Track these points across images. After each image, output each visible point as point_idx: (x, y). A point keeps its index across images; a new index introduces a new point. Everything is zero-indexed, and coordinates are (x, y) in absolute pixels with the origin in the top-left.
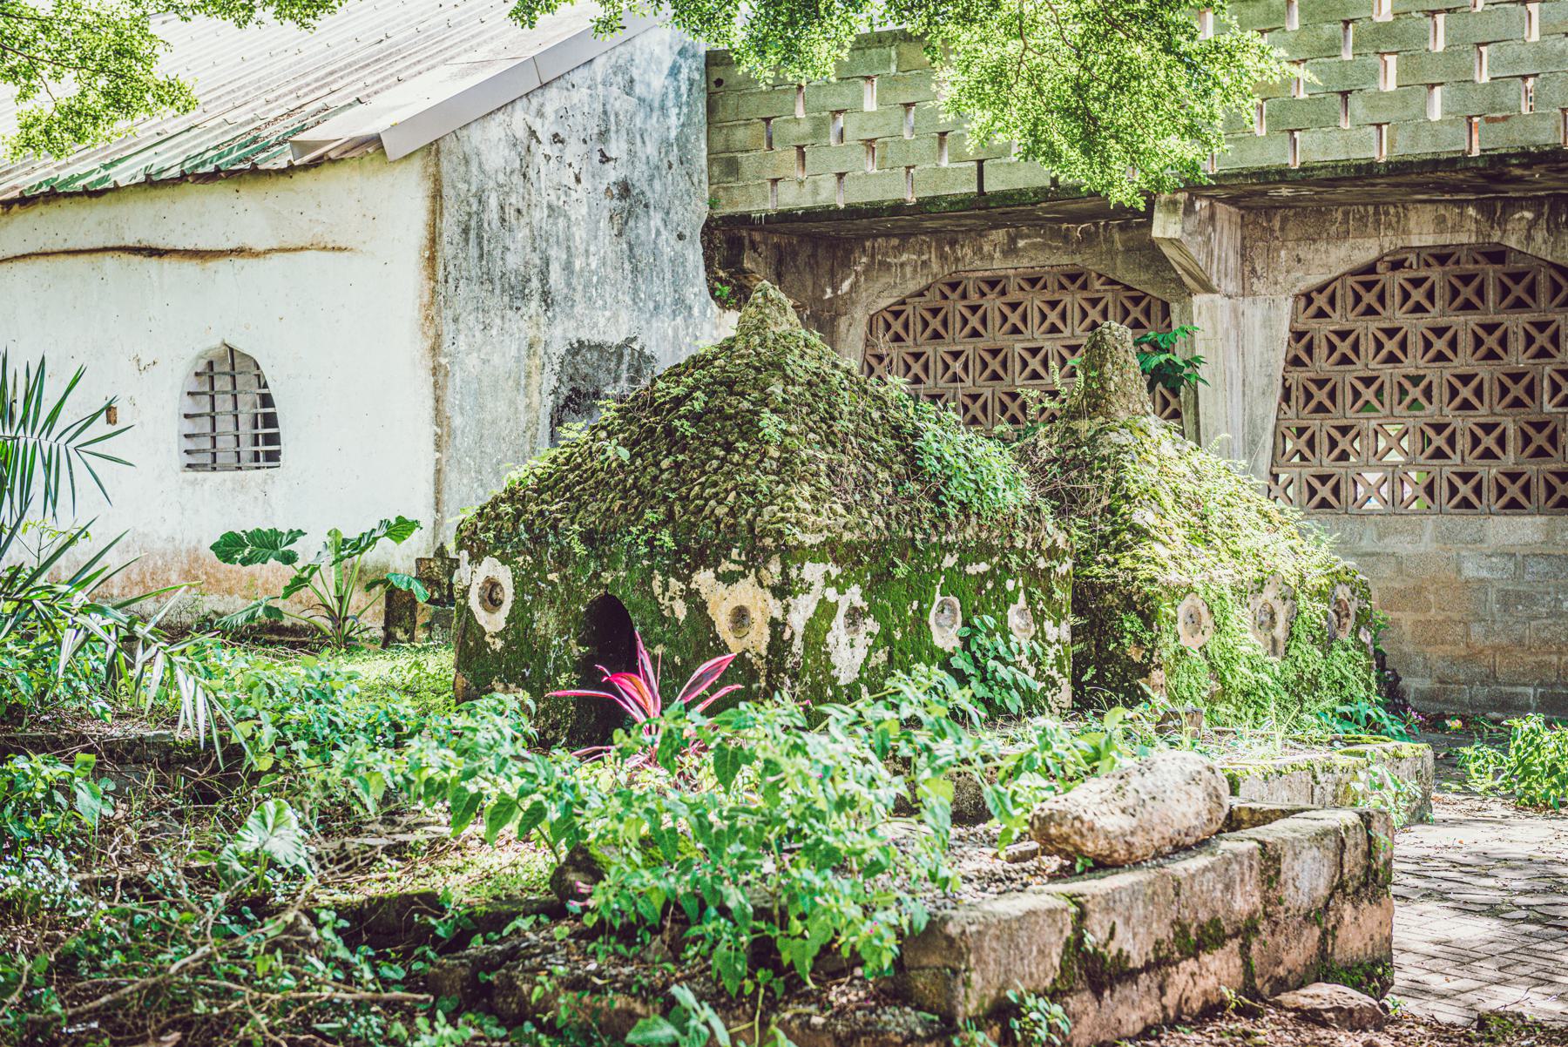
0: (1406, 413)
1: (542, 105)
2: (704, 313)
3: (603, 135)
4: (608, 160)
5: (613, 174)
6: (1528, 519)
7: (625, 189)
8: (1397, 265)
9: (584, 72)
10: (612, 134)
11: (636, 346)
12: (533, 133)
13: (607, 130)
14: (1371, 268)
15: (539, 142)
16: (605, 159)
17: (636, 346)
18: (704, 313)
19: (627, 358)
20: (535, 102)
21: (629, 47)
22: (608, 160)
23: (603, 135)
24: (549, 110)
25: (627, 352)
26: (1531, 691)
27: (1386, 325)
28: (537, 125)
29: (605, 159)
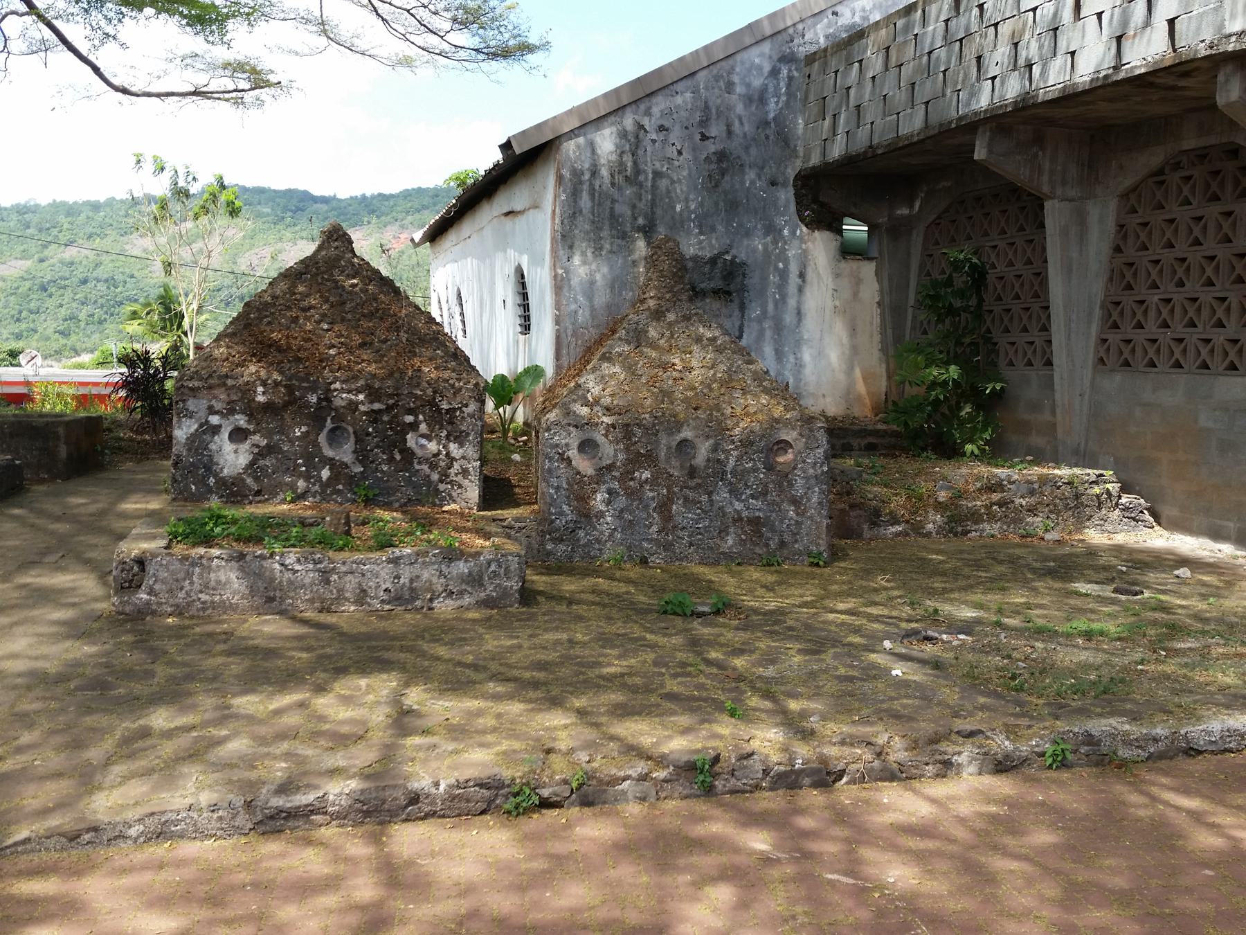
0: (1176, 289)
1: (650, 108)
2: (793, 233)
3: (704, 122)
4: (708, 138)
5: (711, 147)
6: (1239, 379)
7: (722, 156)
8: (1177, 166)
9: (688, 82)
10: (713, 121)
11: (728, 257)
12: (642, 127)
13: (708, 119)
14: (1160, 172)
15: (646, 131)
16: (704, 138)
17: (728, 257)
18: (793, 233)
19: (720, 265)
20: (642, 107)
21: (730, 62)
22: (708, 138)
23: (704, 122)
24: (656, 110)
25: (720, 262)
26: (1231, 525)
27: (1167, 217)
28: (646, 122)
29: (704, 138)
